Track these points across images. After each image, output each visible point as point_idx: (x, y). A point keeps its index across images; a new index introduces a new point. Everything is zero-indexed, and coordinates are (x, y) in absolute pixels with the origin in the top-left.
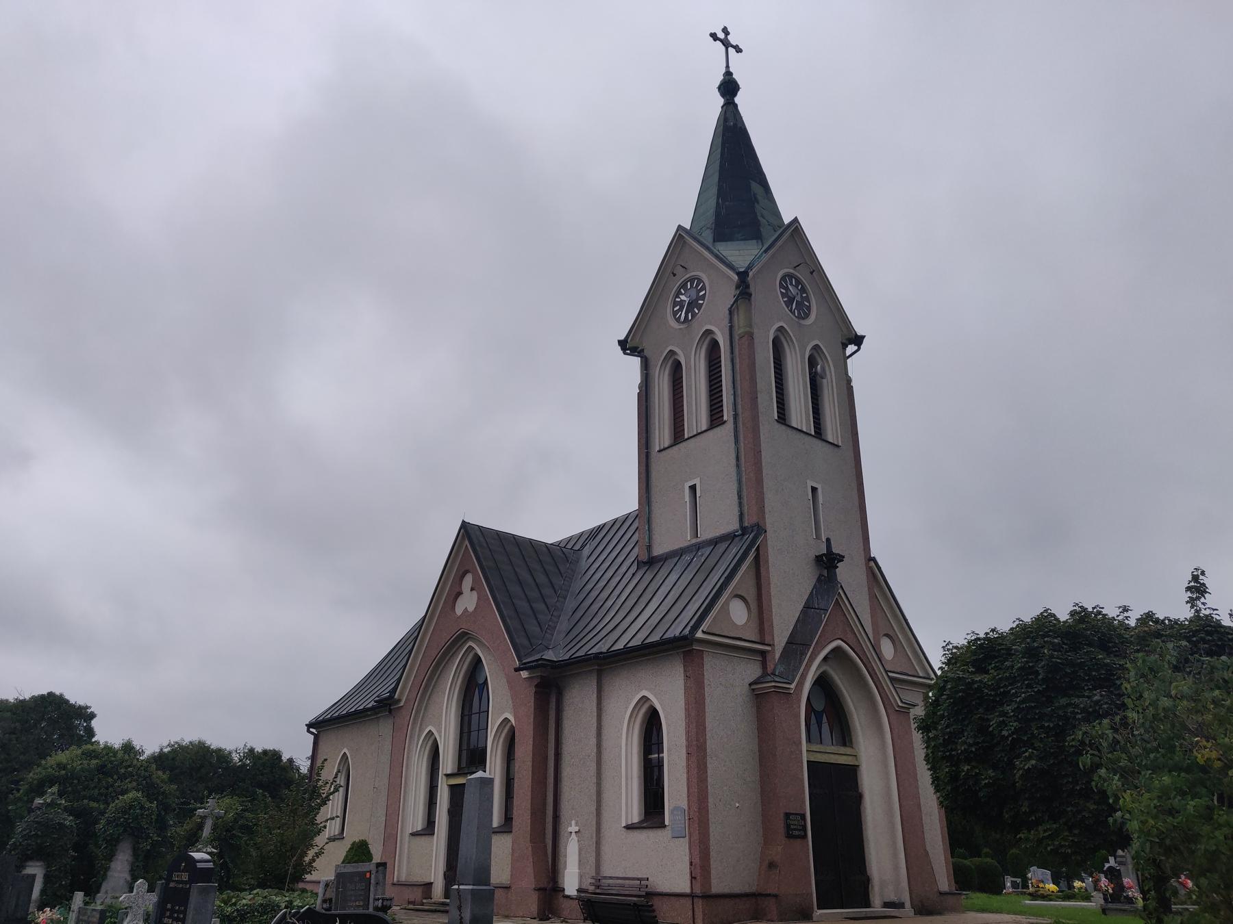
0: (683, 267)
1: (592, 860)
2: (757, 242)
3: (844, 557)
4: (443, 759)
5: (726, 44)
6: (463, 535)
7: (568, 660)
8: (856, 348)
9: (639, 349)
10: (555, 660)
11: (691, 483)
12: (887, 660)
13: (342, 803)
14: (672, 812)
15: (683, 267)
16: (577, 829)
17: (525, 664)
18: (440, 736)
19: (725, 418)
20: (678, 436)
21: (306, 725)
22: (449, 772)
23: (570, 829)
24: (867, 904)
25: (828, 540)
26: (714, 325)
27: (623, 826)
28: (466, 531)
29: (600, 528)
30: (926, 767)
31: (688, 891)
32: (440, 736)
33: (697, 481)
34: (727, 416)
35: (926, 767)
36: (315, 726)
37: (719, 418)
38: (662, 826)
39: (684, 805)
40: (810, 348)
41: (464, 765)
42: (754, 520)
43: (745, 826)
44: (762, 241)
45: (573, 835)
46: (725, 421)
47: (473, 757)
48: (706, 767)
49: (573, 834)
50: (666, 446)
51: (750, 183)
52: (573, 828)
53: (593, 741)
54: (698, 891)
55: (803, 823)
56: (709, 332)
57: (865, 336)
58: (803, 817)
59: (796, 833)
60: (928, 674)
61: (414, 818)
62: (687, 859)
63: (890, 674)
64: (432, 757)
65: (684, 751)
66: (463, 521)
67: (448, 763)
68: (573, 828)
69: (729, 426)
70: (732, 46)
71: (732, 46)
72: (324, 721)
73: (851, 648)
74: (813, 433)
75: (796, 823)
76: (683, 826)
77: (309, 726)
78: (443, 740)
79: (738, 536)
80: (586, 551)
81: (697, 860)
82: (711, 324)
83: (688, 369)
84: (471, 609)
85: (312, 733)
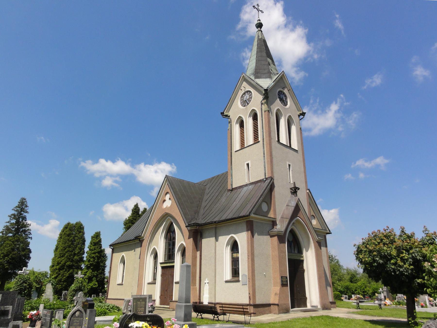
0: (244, 87)
1: (213, 292)
2: (270, 79)
3: (299, 188)
4: (159, 257)
5: (258, 10)
6: (166, 180)
7: (205, 223)
8: (303, 117)
9: (228, 116)
10: (200, 223)
11: (247, 163)
12: (314, 225)
13: (122, 273)
14: (242, 276)
15: (244, 87)
16: (208, 281)
17: (189, 225)
18: (158, 249)
19: (259, 140)
20: (243, 146)
21: (109, 245)
22: (161, 262)
23: (205, 282)
24: (305, 305)
25: (294, 183)
26: (255, 107)
27: (224, 280)
28: (167, 177)
29: (213, 178)
30: (30, 228)
31: (248, 303)
32: (158, 249)
33: (249, 162)
34: (260, 139)
35: (30, 228)
36: (112, 246)
37: (257, 140)
38: (238, 281)
39: (247, 274)
40: (156, 248)
41: (166, 259)
42: (270, 175)
43: (267, 281)
44: (271, 79)
45: (207, 284)
46: (259, 141)
47: (170, 255)
48: (254, 260)
49: (207, 283)
50: (238, 150)
51: (267, 59)
52: (207, 281)
53: (214, 251)
54: (251, 303)
55: (286, 280)
56: (253, 110)
57: (306, 113)
58: (287, 277)
59: (284, 283)
60: (326, 229)
61: (149, 278)
62: (248, 292)
63: (315, 229)
64: (167, 232)
65: (246, 255)
66: (166, 175)
67: (161, 258)
68: (207, 281)
69: (261, 142)
70: (260, 11)
71: (260, 11)
72: (115, 244)
73: (301, 219)
74: (289, 146)
75: (284, 279)
76: (246, 281)
77: (110, 246)
78: (159, 251)
79: (264, 181)
80: (208, 186)
81: (251, 293)
82: (254, 107)
83: (246, 123)
84: (169, 205)
85: (111, 248)
